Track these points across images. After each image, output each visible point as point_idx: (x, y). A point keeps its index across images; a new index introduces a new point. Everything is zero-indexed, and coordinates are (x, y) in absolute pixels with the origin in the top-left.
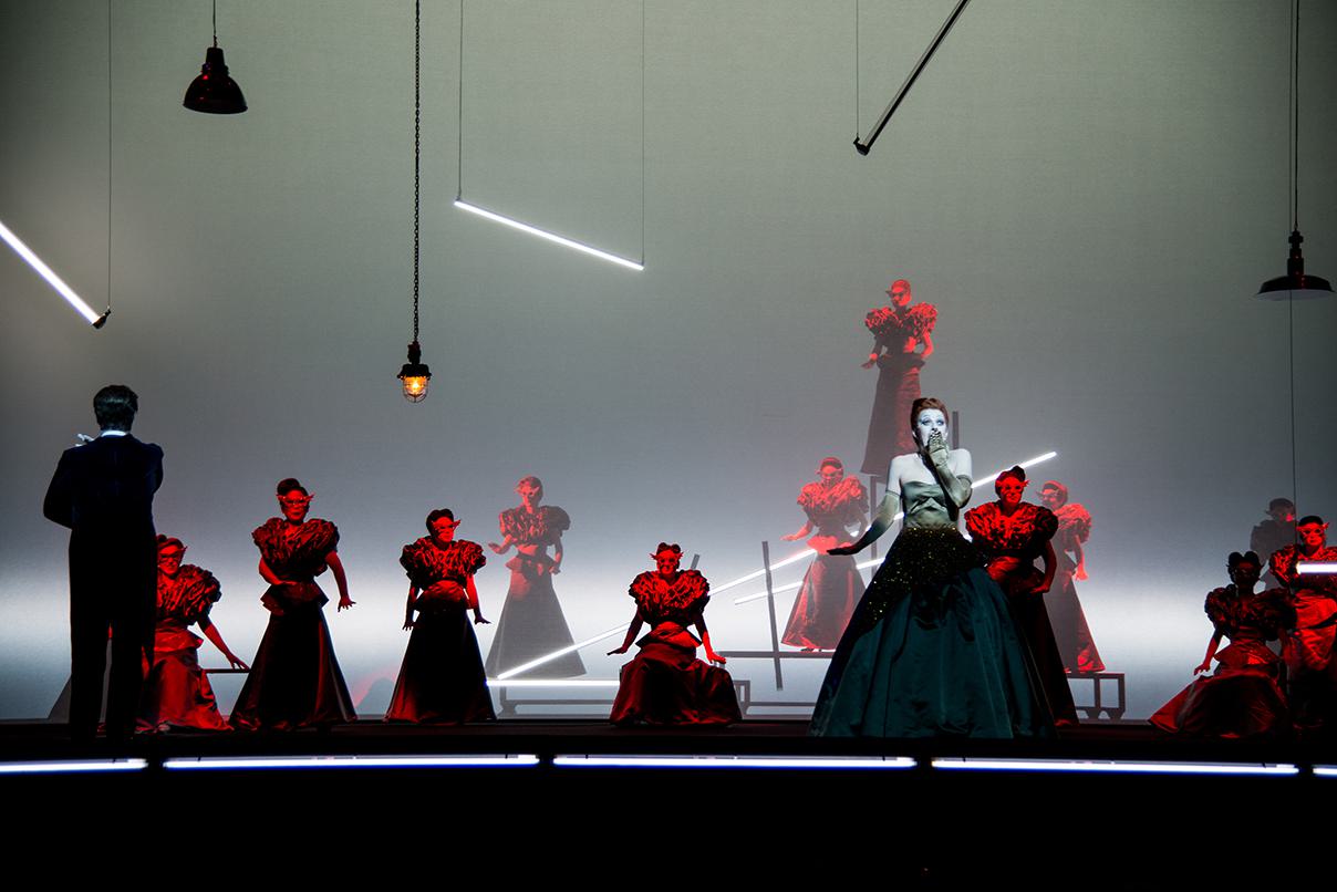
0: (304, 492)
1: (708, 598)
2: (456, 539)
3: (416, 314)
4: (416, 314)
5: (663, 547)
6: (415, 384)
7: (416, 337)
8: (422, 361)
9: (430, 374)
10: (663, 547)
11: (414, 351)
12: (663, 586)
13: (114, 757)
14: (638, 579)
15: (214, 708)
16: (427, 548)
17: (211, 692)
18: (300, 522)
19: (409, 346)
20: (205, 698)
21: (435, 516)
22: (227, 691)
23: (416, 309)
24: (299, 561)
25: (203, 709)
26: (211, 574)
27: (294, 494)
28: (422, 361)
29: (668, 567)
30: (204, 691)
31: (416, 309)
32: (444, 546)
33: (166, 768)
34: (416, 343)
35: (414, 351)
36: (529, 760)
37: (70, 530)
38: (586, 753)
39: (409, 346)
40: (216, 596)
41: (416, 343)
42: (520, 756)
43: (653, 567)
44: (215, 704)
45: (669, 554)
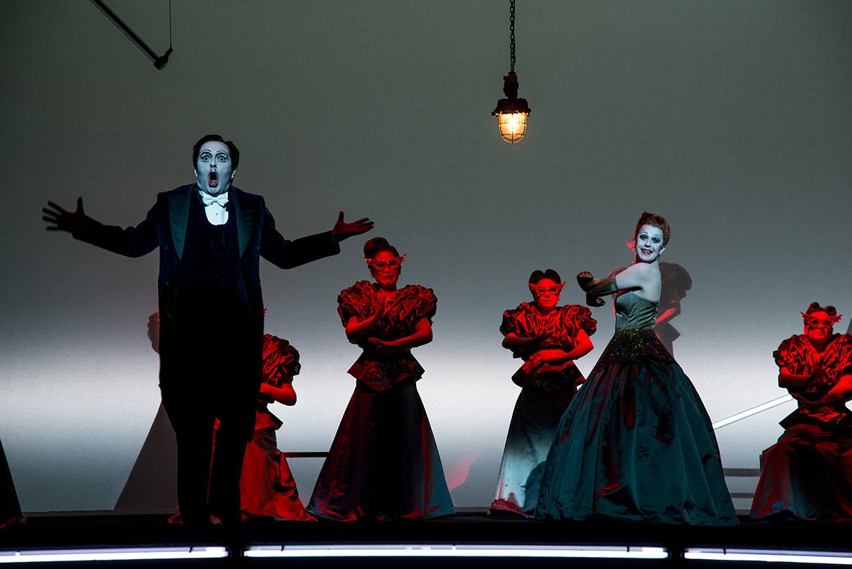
0: (394, 251)
1: (336, 250)
2: (560, 304)
3: (513, 40)
4: (513, 40)
5: (815, 307)
6: (513, 123)
7: (512, 66)
8: (521, 95)
9: (530, 110)
10: (815, 307)
11: (511, 84)
12: (815, 356)
13: (191, 543)
14: (785, 345)
15: (295, 496)
16: (528, 312)
17: (291, 479)
18: (392, 287)
19: (505, 78)
20: (285, 485)
21: (536, 277)
22: (306, 474)
23: (513, 34)
24: (389, 346)
25: (282, 498)
26: (287, 342)
27: (384, 256)
28: (521, 95)
29: (822, 329)
30: (284, 476)
31: (513, 34)
32: (544, 311)
33: (247, 557)
34: (512, 74)
35: (511, 84)
36: (658, 553)
37: (340, 243)
38: (725, 545)
39: (505, 78)
40: (294, 368)
41: (512, 74)
42: (645, 549)
43: (800, 330)
44: (296, 492)
45: (822, 316)
